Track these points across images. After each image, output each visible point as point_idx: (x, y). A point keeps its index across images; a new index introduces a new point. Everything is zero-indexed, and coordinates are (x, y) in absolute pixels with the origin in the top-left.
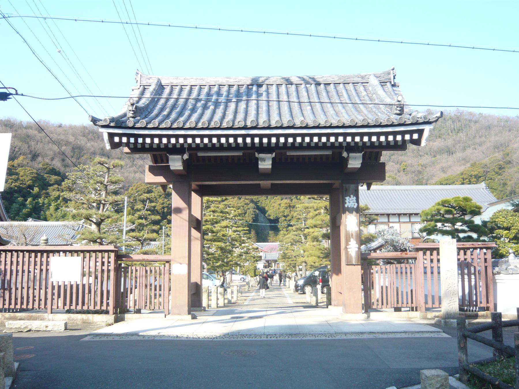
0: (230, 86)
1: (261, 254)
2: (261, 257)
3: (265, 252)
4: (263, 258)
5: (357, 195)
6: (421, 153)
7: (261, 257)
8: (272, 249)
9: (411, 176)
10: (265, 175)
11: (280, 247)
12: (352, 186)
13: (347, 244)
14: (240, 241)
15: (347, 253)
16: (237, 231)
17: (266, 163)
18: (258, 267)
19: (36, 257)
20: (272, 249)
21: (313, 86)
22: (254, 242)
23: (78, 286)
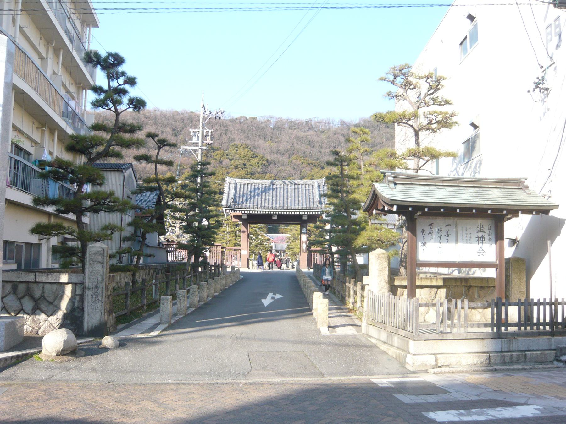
1: (272, 244)
8: (282, 240)
10: (275, 220)
17: (275, 218)
20: (282, 240)
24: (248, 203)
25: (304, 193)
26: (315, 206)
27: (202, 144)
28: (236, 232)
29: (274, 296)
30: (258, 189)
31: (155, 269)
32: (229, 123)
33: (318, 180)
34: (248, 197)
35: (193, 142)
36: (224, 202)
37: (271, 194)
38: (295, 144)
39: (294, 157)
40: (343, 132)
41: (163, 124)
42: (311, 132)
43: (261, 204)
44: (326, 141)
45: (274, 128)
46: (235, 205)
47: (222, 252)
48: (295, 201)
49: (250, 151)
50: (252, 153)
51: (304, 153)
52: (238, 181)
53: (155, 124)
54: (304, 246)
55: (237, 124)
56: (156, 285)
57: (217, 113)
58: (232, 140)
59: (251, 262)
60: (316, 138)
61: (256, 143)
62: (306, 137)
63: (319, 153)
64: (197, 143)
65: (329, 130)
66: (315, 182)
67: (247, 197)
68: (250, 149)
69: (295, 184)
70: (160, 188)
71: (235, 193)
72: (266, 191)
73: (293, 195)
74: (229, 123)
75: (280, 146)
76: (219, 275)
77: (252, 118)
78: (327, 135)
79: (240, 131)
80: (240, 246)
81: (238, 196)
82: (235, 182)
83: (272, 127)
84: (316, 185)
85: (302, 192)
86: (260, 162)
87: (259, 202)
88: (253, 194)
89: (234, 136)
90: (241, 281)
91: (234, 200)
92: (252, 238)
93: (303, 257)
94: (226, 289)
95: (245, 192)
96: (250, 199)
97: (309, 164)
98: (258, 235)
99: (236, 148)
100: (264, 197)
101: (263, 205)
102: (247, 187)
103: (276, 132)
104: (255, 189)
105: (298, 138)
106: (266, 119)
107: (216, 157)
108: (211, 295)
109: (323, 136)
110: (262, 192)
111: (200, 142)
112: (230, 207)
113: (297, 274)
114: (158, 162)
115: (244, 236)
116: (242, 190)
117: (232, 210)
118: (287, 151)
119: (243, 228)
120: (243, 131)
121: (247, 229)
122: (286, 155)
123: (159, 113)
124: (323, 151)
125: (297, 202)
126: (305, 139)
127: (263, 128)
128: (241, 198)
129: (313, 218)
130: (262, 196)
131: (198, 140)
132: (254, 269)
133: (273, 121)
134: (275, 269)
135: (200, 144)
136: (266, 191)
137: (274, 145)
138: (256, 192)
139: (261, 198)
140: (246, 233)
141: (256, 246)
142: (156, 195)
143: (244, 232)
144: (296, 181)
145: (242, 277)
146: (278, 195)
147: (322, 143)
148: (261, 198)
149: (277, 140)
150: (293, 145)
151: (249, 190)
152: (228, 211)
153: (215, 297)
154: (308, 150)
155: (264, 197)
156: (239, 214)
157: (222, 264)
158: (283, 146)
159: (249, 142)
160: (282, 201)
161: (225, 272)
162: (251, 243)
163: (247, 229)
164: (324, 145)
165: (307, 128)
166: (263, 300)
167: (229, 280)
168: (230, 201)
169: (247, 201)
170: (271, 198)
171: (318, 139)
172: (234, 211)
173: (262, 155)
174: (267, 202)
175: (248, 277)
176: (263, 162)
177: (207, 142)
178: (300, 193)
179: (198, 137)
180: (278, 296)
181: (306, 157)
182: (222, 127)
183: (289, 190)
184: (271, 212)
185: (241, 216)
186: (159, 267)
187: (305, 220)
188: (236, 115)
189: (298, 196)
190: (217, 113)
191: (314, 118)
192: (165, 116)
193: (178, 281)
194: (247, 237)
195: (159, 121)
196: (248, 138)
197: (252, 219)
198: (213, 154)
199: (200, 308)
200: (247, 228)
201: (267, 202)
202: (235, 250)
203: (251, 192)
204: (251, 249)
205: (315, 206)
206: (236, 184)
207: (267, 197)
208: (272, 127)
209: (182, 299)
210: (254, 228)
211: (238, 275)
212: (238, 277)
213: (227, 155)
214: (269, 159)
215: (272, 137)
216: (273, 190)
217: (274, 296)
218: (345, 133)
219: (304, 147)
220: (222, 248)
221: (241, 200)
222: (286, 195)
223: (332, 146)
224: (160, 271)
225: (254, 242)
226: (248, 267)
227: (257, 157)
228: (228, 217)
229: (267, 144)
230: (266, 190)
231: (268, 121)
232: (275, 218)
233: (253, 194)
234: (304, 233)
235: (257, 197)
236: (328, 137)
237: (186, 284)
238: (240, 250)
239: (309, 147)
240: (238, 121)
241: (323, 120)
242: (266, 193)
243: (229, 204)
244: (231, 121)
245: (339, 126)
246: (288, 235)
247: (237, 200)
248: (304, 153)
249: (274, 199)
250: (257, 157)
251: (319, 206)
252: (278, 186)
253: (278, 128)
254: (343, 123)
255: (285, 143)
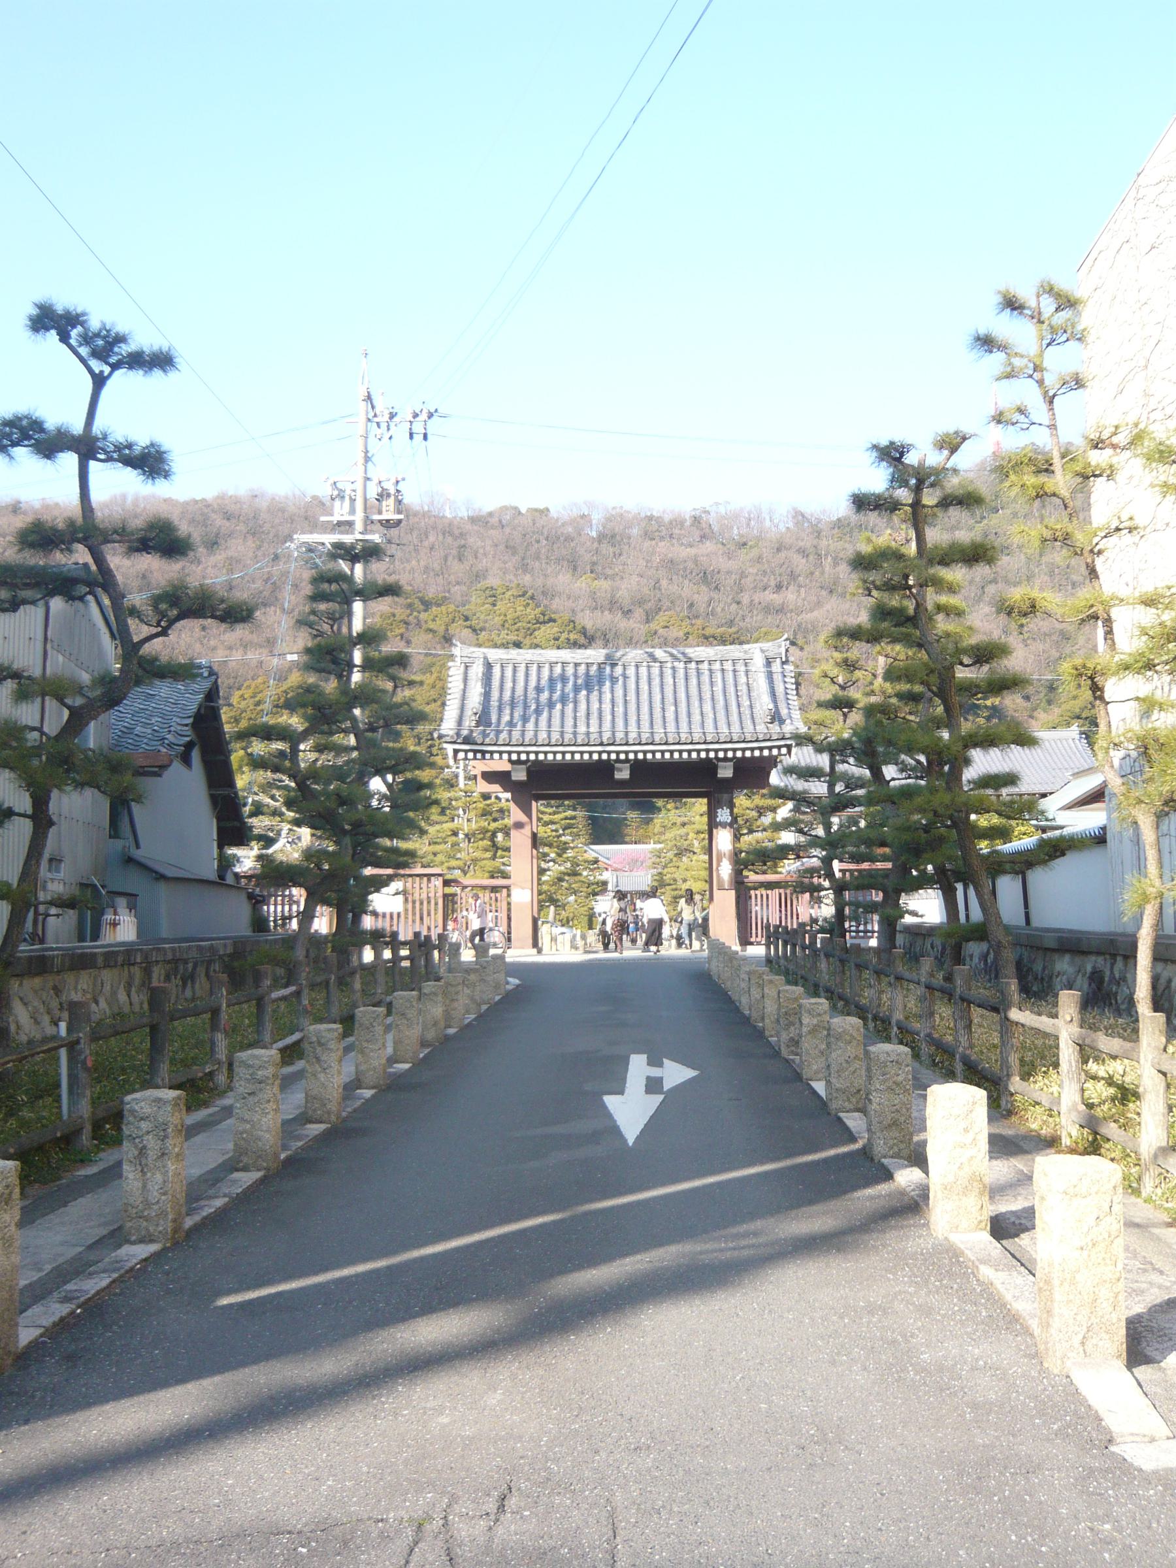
0: (576, 665)
1: (606, 876)
2: (605, 883)
3: (616, 870)
4: (610, 887)
5: (731, 806)
6: (1074, 577)
7: (605, 883)
8: (634, 863)
9: (1041, 647)
10: (622, 783)
11: (654, 859)
12: (726, 796)
13: (719, 865)
14: (558, 847)
15: (718, 875)
16: (553, 823)
17: (623, 774)
18: (597, 910)
19: (413, 883)
20: (634, 863)
21: (682, 665)
22: (586, 845)
23: (399, 914)
24: (530, 726)
25: (718, 688)
26: (761, 728)
27: (366, 525)
28: (494, 835)
29: (655, 1072)
30: (564, 679)
31: (175, 961)
32: (468, 527)
33: (766, 645)
34: (527, 708)
35: (336, 518)
36: (448, 726)
37: (607, 696)
38: (664, 583)
39: (661, 618)
40: (801, 544)
41: (276, 536)
42: (709, 546)
43: (575, 726)
44: (753, 571)
45: (601, 537)
46: (485, 735)
47: (445, 896)
48: (689, 715)
49: (532, 605)
50: (538, 610)
51: (692, 605)
52: (494, 654)
53: (254, 534)
54: (725, 870)
55: (493, 527)
56: (72, 1046)
57: (416, 415)
58: (478, 576)
59: (544, 930)
60: (723, 563)
61: (550, 582)
62: (696, 562)
63: (734, 606)
64: (350, 524)
65: (759, 539)
66: (756, 652)
67: (526, 706)
68: (532, 598)
69: (689, 661)
70: (104, 580)
71: (487, 695)
72: (588, 686)
73: (682, 696)
74: (468, 527)
75: (618, 589)
76: (431, 974)
77: (536, 510)
78: (754, 553)
79: (502, 547)
80: (505, 876)
81: (494, 703)
82: (485, 658)
83: (594, 534)
84: (758, 662)
85: (712, 684)
86: (564, 636)
87: (569, 722)
88: (545, 696)
89: (484, 563)
90: (513, 999)
91: (483, 718)
92: (545, 855)
93: (724, 906)
94: (447, 1038)
95: (520, 691)
96: (538, 712)
97: (706, 638)
98: (563, 849)
99: (493, 596)
100: (583, 706)
101: (582, 729)
102: (527, 675)
103: (607, 549)
104: (551, 680)
105: (671, 564)
106: (575, 513)
107: (432, 625)
108: (370, 1078)
109: (744, 555)
110: (577, 689)
111: (358, 518)
112: (467, 740)
113: (715, 967)
114: (88, 447)
115: (520, 841)
116: (509, 685)
117: (475, 752)
118: (641, 602)
119: (517, 814)
120: (511, 548)
121: (530, 816)
122: (639, 613)
123: (264, 505)
124: (745, 600)
125: (696, 718)
126: (690, 565)
127: (569, 539)
128: (507, 711)
129: (752, 772)
130: (576, 702)
131: (352, 511)
132: (563, 947)
133: (597, 517)
134: (632, 952)
135: (359, 526)
136: (588, 686)
137: (604, 584)
138: (557, 690)
139: (575, 710)
140: (527, 831)
141: (560, 880)
142: (196, 693)
143: (519, 825)
144: (690, 651)
145: (514, 981)
146: (632, 697)
147: (743, 575)
148: (575, 710)
149: (609, 572)
150: (656, 586)
151: (533, 683)
152: (461, 755)
153: (393, 1086)
154: (701, 596)
155: (583, 706)
156: (504, 766)
157: (442, 937)
158: (627, 588)
159: (527, 579)
160: (645, 716)
161: (456, 966)
162: (542, 872)
163: (530, 816)
164: (748, 582)
165: (697, 535)
166: (610, 1101)
167: (463, 1000)
168: (469, 722)
169: (525, 720)
170: (607, 707)
171: (732, 565)
172: (483, 753)
173: (567, 616)
174: (594, 721)
175: (536, 984)
176: (572, 636)
177: (385, 516)
178: (706, 688)
179: (353, 501)
180: (675, 1074)
181: (697, 617)
182: (449, 540)
183: (669, 680)
184: (611, 753)
185: (507, 774)
186: (194, 954)
187: (725, 781)
188: (487, 504)
189: (701, 699)
190: (416, 415)
191: (717, 504)
192: (283, 510)
193: (224, 1016)
194: (529, 842)
195: (267, 527)
196: (525, 568)
197: (544, 781)
198: (423, 616)
199: (294, 1166)
200: (527, 812)
201: (594, 721)
202: (494, 889)
203: (539, 690)
204: (545, 887)
205: (761, 728)
206: (489, 666)
207: (595, 706)
208: (594, 534)
209: (151, 1142)
210: (548, 816)
211: (501, 976)
212: (497, 986)
213: (467, 619)
214: (589, 626)
215: (594, 564)
216: (614, 681)
217: (655, 1072)
218: (808, 545)
219: (688, 590)
220: (447, 883)
221: (506, 718)
222: (657, 697)
223: (773, 583)
224: (201, 971)
225: (554, 869)
226: (535, 944)
227: (554, 621)
228: (463, 774)
229: (583, 584)
230: (592, 682)
231: (583, 516)
232: (623, 774)
233: (545, 696)
234: (724, 825)
235: (559, 706)
236: (759, 559)
237: (269, 1026)
238: (508, 888)
239: (704, 588)
240: (494, 520)
241: (742, 510)
242: (589, 691)
243: (465, 733)
244: (473, 520)
245: (791, 525)
246: (651, 846)
247: (494, 719)
248: (692, 605)
249: (620, 710)
250: (554, 621)
251: (775, 729)
252: (631, 671)
253: (613, 536)
254: (799, 516)
255: (635, 578)
